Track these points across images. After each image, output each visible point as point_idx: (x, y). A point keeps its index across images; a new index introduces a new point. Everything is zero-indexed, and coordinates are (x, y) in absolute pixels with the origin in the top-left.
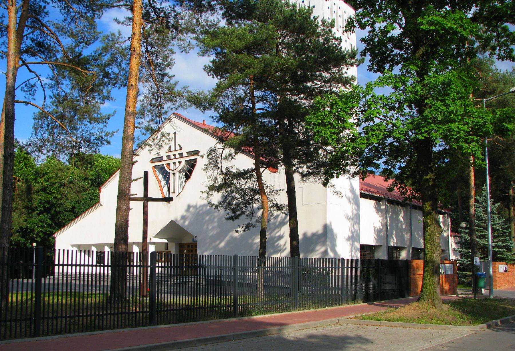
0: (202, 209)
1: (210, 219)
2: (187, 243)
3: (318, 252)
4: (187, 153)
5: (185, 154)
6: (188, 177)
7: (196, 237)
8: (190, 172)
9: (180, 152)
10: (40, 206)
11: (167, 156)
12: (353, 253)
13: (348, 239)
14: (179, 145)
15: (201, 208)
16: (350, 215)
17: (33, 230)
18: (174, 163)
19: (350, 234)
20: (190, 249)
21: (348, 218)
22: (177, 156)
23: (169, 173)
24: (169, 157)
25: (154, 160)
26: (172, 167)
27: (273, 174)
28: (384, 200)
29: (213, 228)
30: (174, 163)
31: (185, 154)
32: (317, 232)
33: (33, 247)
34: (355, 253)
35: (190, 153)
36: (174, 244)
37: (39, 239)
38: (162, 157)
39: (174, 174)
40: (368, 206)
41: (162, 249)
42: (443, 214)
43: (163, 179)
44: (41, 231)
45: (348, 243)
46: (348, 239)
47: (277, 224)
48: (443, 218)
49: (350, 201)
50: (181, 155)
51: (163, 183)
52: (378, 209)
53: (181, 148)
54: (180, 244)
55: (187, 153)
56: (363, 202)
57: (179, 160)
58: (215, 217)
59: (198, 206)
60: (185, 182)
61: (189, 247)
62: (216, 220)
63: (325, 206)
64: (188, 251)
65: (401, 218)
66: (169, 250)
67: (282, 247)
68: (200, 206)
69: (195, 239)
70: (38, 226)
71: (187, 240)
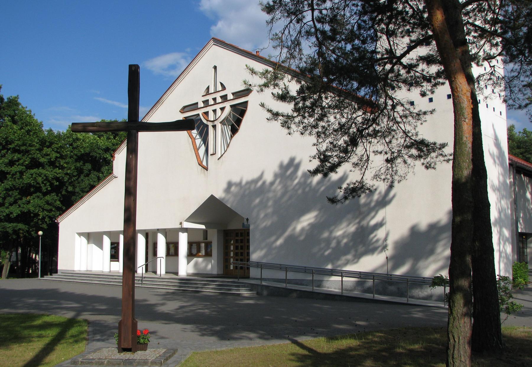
0: (249, 188)
1: (261, 202)
2: (235, 230)
3: (441, 256)
4: (233, 94)
5: (230, 97)
6: (234, 131)
7: (247, 219)
8: (239, 122)
9: (223, 93)
10: (45, 185)
11: (204, 102)
14: (222, 84)
15: (248, 186)
17: (37, 215)
18: (215, 111)
20: (239, 238)
22: (219, 100)
23: (207, 126)
24: (206, 103)
25: (186, 109)
26: (211, 117)
29: (266, 215)
30: (215, 111)
31: (230, 97)
32: (438, 222)
33: (39, 236)
34: (503, 247)
35: (237, 95)
36: (215, 231)
37: (45, 226)
38: (197, 103)
39: (214, 127)
41: (200, 238)
43: (198, 137)
44: (47, 215)
47: (373, 204)
50: (224, 98)
51: (199, 141)
53: (224, 88)
54: (224, 230)
55: (233, 94)
57: (222, 106)
58: (268, 200)
59: (244, 182)
60: (230, 140)
61: (237, 235)
62: (270, 203)
64: (237, 241)
66: (209, 239)
67: (380, 242)
68: (247, 183)
69: (246, 223)
70: (43, 209)
71: (235, 226)
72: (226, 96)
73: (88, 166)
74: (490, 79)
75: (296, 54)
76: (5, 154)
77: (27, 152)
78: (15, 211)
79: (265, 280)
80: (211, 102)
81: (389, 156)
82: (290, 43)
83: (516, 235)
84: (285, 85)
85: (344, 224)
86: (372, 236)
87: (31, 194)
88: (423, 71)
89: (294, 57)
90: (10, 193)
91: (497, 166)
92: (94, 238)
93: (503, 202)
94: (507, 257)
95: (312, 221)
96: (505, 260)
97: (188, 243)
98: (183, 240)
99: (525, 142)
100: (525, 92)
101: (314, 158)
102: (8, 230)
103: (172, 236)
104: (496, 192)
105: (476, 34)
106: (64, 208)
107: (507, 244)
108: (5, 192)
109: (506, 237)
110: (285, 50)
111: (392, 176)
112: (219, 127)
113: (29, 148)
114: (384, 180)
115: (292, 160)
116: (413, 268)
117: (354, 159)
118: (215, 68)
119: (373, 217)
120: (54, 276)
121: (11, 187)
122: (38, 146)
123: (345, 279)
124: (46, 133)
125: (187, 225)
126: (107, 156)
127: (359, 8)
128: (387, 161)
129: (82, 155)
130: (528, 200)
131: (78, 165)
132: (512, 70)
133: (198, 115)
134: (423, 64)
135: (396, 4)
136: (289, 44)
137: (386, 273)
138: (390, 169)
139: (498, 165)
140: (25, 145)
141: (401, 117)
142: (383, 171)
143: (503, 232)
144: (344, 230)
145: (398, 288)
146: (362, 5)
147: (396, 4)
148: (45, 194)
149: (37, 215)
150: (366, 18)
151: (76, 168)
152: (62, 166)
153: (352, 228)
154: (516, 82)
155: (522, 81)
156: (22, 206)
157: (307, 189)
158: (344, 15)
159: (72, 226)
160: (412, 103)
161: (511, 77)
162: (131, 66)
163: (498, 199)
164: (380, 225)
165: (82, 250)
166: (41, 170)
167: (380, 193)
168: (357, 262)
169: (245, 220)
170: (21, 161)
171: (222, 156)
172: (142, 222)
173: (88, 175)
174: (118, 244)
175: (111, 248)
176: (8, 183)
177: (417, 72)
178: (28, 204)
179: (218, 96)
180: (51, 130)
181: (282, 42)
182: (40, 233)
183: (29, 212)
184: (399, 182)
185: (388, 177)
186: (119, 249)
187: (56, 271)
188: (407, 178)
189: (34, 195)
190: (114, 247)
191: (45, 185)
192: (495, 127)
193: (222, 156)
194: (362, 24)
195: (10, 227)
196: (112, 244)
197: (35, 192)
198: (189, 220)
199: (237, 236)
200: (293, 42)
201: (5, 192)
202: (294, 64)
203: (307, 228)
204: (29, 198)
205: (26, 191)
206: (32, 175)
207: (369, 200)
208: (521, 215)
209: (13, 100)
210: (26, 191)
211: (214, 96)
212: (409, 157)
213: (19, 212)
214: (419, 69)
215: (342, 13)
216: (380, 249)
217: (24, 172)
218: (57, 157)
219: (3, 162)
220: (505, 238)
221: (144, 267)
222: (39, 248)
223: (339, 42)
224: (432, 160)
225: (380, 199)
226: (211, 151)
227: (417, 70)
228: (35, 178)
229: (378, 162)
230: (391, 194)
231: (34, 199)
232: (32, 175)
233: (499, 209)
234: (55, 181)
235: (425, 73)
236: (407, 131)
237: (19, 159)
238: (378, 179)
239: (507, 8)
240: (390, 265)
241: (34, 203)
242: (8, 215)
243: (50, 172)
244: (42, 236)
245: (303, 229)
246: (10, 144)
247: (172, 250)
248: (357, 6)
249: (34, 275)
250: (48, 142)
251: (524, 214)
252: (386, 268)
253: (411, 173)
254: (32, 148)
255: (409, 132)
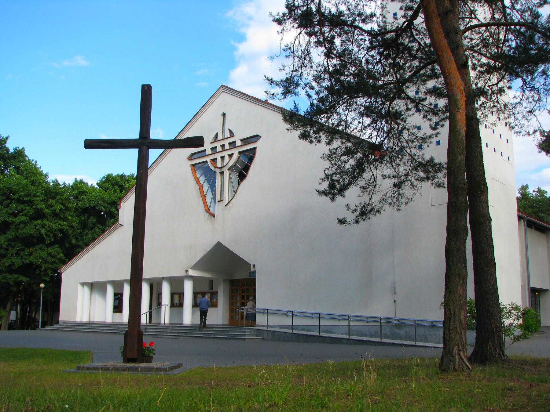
4: (242, 140)
5: (238, 143)
6: (242, 177)
7: (254, 266)
8: (247, 168)
9: (231, 140)
14: (230, 131)
18: (223, 158)
22: (227, 147)
23: (215, 172)
26: (219, 164)
30: (223, 158)
31: (238, 143)
33: (41, 288)
35: (245, 141)
37: (48, 279)
39: (222, 173)
51: (206, 187)
53: (232, 134)
55: (242, 140)
57: (230, 152)
70: (46, 262)
71: (241, 275)
72: (234, 142)
73: (93, 219)
74: (494, 106)
75: (306, 62)
76: (8, 204)
77: (31, 203)
78: (18, 263)
79: (272, 326)
80: (219, 149)
81: (396, 181)
82: (300, 53)
84: (295, 103)
87: (33, 245)
88: (431, 104)
89: (306, 66)
90: (13, 244)
92: (97, 287)
97: (193, 293)
98: (188, 288)
100: (529, 118)
101: (324, 180)
102: (9, 281)
103: (177, 284)
105: (481, 69)
106: (67, 260)
108: (7, 243)
110: (297, 60)
111: (398, 199)
112: (227, 173)
113: (33, 199)
114: (390, 204)
117: (361, 182)
118: (224, 115)
120: (56, 326)
121: (13, 238)
122: (43, 197)
123: (352, 324)
124: (51, 184)
125: (191, 273)
126: (113, 210)
127: (367, 43)
128: (395, 185)
129: (87, 208)
131: (83, 218)
132: (514, 97)
133: (206, 162)
134: (431, 97)
135: (402, 38)
136: (300, 55)
138: (397, 193)
140: (30, 196)
141: (407, 142)
142: (390, 194)
145: (406, 332)
146: (369, 39)
147: (402, 38)
148: (49, 246)
149: (39, 267)
150: (372, 53)
151: (81, 222)
152: (66, 218)
154: (519, 108)
155: (525, 108)
156: (24, 257)
158: (352, 50)
159: (74, 278)
160: (419, 128)
161: (514, 104)
162: (143, 86)
165: (85, 298)
166: (45, 222)
169: (252, 266)
170: (25, 212)
171: (229, 202)
172: (149, 271)
173: (92, 228)
174: (122, 295)
175: (115, 299)
176: (11, 234)
177: (425, 106)
178: (30, 255)
179: (226, 143)
180: (57, 181)
181: (293, 52)
182: (42, 285)
183: (31, 264)
184: (406, 204)
185: (395, 200)
186: (122, 300)
187: (58, 322)
188: (413, 200)
189: (37, 247)
190: (118, 298)
191: (48, 236)
193: (229, 202)
194: (370, 58)
195: (12, 278)
196: (116, 295)
197: (37, 244)
198: (194, 267)
199: (243, 285)
200: (303, 52)
201: (7, 243)
202: (305, 72)
204: (31, 249)
205: (30, 242)
206: (36, 226)
209: (19, 151)
210: (30, 242)
211: (222, 143)
212: (417, 180)
213: (21, 264)
214: (426, 103)
215: (350, 48)
217: (28, 222)
218: (61, 209)
219: (6, 212)
221: (148, 314)
222: (39, 301)
223: (348, 76)
224: (440, 181)
226: (218, 198)
227: (425, 104)
228: (39, 229)
229: (386, 185)
231: (36, 250)
232: (36, 226)
234: (58, 233)
235: (432, 107)
236: (412, 154)
237: (22, 210)
238: (384, 203)
239: (510, 43)
241: (37, 255)
242: (10, 265)
243: (55, 225)
244: (43, 288)
246: (14, 194)
247: (177, 303)
248: (365, 41)
249: (35, 328)
250: (54, 192)
253: (418, 194)
254: (38, 199)
255: (414, 155)
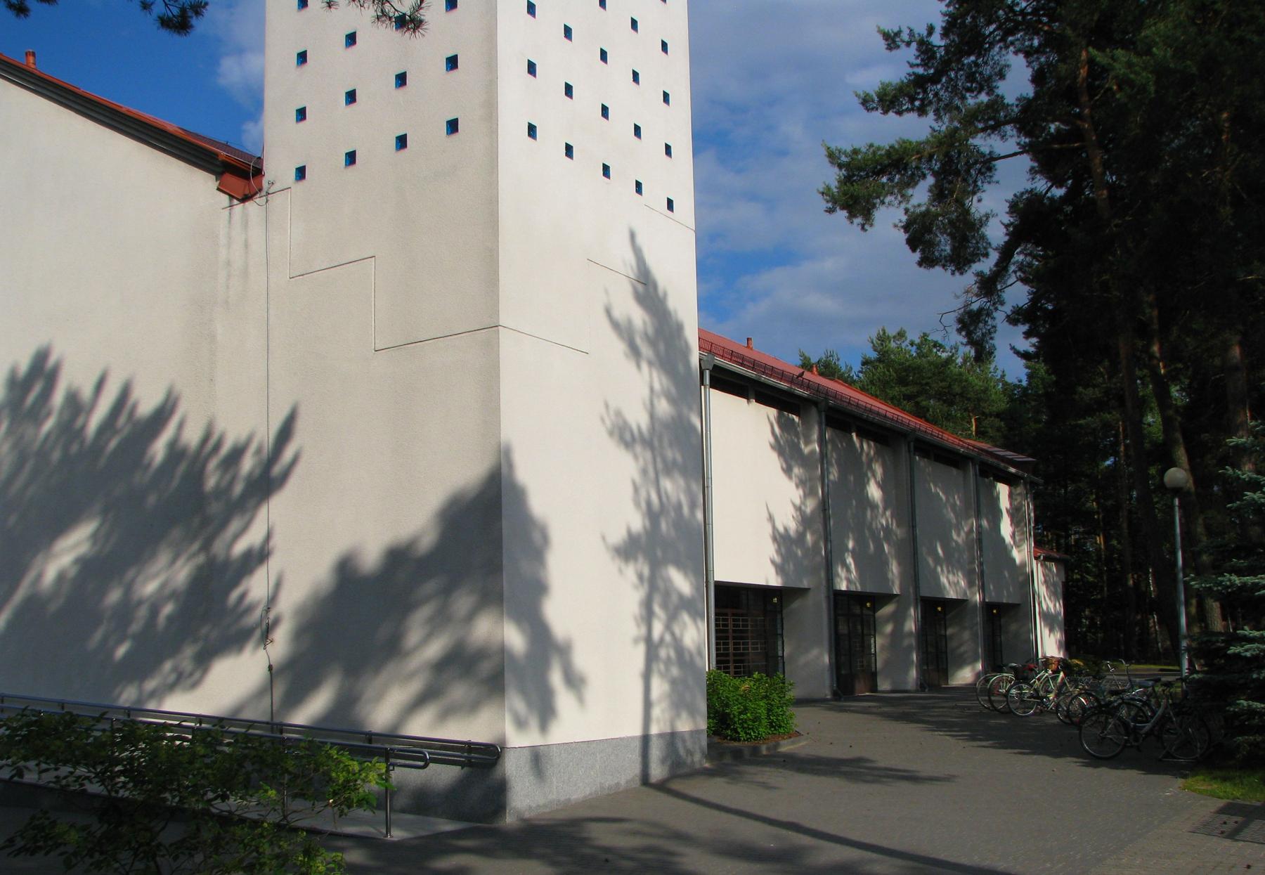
12: (658, 628)
13: (629, 550)
16: (638, 418)
19: (637, 522)
21: (624, 436)
27: (238, 208)
28: (814, 411)
34: (668, 627)
40: (741, 432)
42: (1010, 481)
45: (630, 571)
46: (629, 550)
47: (238, 489)
48: (1011, 496)
49: (635, 351)
52: (788, 451)
56: (721, 404)
63: (491, 348)
65: (874, 492)
83: (828, 597)
85: (163, 558)
86: (234, 595)
91: (644, 366)
93: (667, 484)
94: (683, 657)
95: (84, 549)
96: (675, 671)
99: (918, 369)
104: (638, 448)
107: (686, 617)
109: (681, 596)
115: (41, 358)
116: (346, 703)
119: (237, 536)
130: (873, 506)
137: (266, 718)
139: (650, 363)
143: (668, 581)
144: (164, 576)
153: (182, 573)
157: (75, 448)
163: (644, 472)
164: (259, 556)
167: (259, 451)
168: (195, 685)
192: (640, 240)
203: (72, 573)
207: (228, 477)
208: (851, 545)
216: (258, 633)
220: (674, 599)
225: (257, 472)
230: (288, 454)
233: (649, 504)
240: (279, 691)
245: (61, 577)
251: (860, 542)
252: (266, 702)
